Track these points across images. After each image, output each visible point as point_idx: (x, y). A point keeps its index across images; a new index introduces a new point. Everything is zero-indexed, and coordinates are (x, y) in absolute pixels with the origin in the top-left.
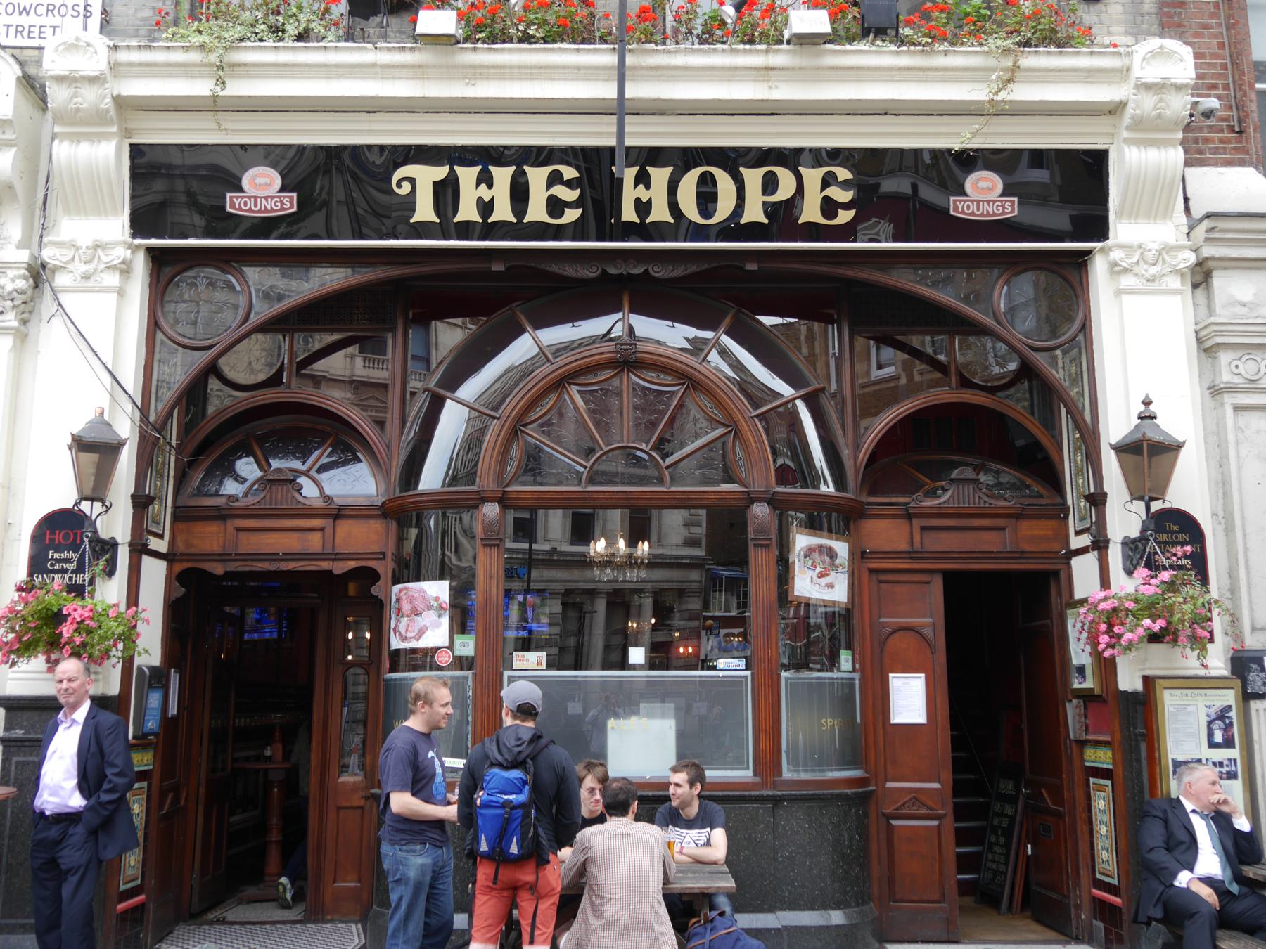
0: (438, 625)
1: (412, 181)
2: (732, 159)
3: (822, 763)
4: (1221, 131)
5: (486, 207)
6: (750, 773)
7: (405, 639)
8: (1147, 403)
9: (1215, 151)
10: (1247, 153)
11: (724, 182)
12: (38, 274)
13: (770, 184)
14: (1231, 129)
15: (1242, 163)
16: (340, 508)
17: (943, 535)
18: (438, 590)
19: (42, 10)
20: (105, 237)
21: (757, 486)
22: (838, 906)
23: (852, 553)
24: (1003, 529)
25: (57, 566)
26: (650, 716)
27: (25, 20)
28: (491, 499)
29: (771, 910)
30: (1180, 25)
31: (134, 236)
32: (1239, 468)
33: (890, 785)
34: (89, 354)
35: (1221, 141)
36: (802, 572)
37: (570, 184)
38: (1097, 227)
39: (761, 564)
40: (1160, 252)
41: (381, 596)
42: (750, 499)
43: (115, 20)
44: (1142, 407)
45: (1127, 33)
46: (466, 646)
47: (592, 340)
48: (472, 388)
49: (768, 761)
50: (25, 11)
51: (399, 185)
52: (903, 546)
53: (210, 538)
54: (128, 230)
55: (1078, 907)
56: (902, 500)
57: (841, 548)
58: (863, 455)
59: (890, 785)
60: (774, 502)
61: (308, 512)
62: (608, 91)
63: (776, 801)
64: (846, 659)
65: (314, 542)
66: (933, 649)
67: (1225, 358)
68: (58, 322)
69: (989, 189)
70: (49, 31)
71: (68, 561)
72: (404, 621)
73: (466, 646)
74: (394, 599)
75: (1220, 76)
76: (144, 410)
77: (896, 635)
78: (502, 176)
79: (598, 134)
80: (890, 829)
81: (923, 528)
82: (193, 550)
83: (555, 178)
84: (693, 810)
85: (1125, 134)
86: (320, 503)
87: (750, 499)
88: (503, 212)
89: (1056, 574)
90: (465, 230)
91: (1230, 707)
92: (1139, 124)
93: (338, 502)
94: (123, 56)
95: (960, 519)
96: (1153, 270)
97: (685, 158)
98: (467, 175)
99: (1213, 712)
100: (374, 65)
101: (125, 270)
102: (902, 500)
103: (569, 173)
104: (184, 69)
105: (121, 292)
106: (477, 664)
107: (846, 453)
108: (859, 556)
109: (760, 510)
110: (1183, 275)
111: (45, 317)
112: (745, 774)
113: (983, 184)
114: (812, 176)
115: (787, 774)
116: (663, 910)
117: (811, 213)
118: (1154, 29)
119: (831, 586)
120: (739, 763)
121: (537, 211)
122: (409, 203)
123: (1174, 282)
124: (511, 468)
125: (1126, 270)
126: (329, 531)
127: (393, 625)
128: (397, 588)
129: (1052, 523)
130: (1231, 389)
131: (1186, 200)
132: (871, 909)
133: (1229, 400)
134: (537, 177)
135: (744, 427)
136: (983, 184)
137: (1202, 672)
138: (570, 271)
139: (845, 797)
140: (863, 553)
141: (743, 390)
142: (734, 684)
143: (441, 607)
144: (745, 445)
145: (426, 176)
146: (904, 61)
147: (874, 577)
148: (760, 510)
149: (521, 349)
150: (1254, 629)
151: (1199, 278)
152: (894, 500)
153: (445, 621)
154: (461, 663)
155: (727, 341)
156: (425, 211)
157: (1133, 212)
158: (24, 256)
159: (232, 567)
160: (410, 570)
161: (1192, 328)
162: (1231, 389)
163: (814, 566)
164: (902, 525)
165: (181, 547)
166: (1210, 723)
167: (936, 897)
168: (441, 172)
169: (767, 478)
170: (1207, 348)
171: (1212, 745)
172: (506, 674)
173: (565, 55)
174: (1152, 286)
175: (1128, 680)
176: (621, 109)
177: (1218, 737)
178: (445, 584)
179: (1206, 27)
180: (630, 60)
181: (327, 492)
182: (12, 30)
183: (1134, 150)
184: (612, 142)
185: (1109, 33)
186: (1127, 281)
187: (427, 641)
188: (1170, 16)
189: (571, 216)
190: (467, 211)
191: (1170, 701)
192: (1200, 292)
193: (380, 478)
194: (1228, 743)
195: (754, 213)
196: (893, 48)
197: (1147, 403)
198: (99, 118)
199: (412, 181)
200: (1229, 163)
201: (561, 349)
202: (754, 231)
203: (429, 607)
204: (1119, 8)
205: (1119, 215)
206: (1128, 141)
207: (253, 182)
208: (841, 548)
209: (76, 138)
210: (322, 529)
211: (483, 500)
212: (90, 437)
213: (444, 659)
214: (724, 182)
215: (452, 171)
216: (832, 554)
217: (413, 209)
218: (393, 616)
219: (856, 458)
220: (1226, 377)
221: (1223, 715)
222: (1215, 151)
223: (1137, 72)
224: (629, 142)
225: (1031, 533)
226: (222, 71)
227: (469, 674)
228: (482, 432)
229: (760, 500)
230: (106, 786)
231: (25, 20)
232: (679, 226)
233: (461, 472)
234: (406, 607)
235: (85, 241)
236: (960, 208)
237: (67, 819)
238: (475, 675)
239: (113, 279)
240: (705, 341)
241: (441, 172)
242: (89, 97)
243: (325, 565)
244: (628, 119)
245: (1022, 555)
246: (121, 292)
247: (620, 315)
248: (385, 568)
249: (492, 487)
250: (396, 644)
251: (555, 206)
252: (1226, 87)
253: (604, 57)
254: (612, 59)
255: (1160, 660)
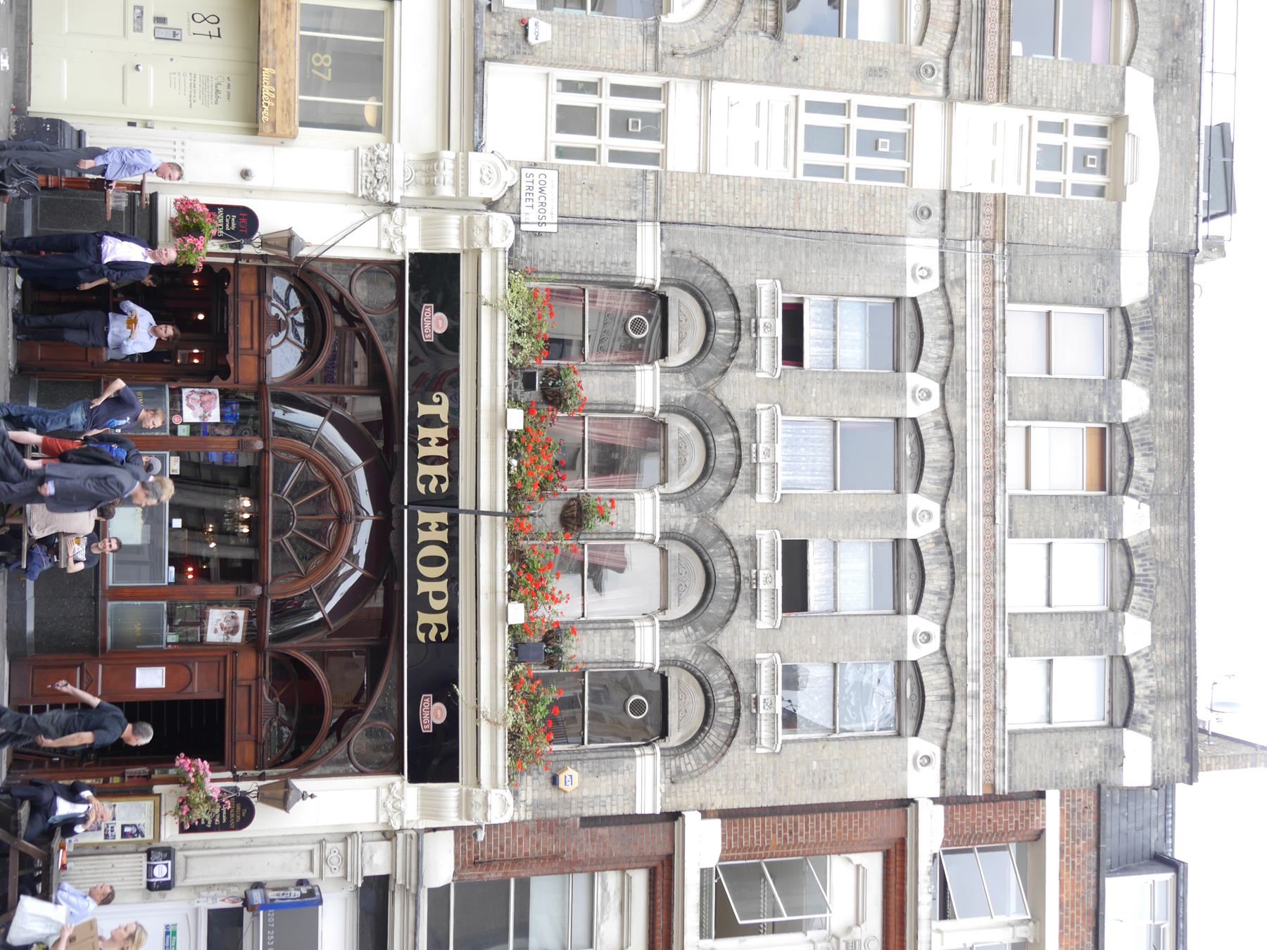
0: (195, 416)
1: (440, 403)
2: (452, 577)
3: (114, 626)
4: (476, 852)
5: (426, 442)
6: (111, 584)
7: (188, 397)
8: (312, 796)
9: (463, 848)
10: (463, 867)
11: (442, 570)
12: (390, 205)
13: (438, 595)
14: (477, 858)
15: (456, 864)
16: (265, 359)
17: (246, 699)
18: (215, 416)
19: (542, 200)
20: (407, 241)
21: (270, 589)
22: (36, 631)
23: (236, 644)
24: (249, 733)
25: (227, 220)
26: (143, 532)
27: (536, 191)
28: (265, 444)
29: (36, 594)
30: (539, 831)
31: (411, 254)
32: (277, 852)
33: (100, 667)
34: (344, 234)
35: (469, 852)
36: (223, 614)
37: (438, 488)
38: (413, 779)
39: (228, 589)
40: (399, 810)
41: (213, 381)
42: (263, 584)
43: (538, 239)
44: (309, 794)
45: (533, 800)
46: (183, 431)
47: (356, 501)
48: (332, 434)
49: (118, 594)
50: (542, 190)
51: (437, 396)
52: (239, 675)
53: (247, 285)
54: (414, 252)
55: (27, 773)
56: (267, 675)
57: (238, 638)
58: (294, 653)
59: (100, 667)
60: (262, 598)
61: (261, 341)
62: (484, 506)
63: (96, 598)
64: (173, 638)
65: (245, 344)
66: (178, 693)
67: (340, 846)
68: (361, 217)
69: (437, 716)
70: (530, 203)
71: (230, 225)
72: (198, 397)
73: (183, 431)
74: (211, 390)
75: (508, 853)
76: (317, 259)
77: (187, 672)
78: (443, 451)
79: (465, 501)
80: (76, 667)
81: (250, 686)
82: (240, 277)
83: (441, 479)
84: (95, 551)
85: (464, 789)
86: (267, 347)
87: (263, 584)
88: (423, 451)
89: (223, 764)
90: (414, 432)
91: (143, 836)
92: (469, 794)
93: (268, 357)
94: (501, 255)
95: (254, 708)
96: (389, 806)
97: (452, 546)
98: (443, 433)
99: (141, 827)
100: (497, 385)
101: (390, 250)
102: (267, 675)
103: (444, 487)
104: (494, 287)
105: (378, 248)
106: (174, 437)
107: (294, 643)
108: (233, 649)
109: (258, 590)
110: (387, 824)
111: (364, 208)
112: (110, 581)
113: (439, 712)
114: (443, 619)
115: (110, 604)
116: (54, 532)
117: (423, 618)
118: (536, 815)
119: (216, 631)
120: (115, 579)
121: (423, 470)
122: (428, 401)
123: (383, 819)
124: (283, 455)
125: (390, 790)
126: (251, 352)
127: (196, 390)
128: (216, 392)
129: (252, 761)
130: (322, 848)
131: (434, 830)
132: (31, 652)
133: (316, 847)
134: (442, 470)
135: (305, 582)
136: (439, 712)
137: (163, 813)
138: (393, 487)
139: (97, 635)
140: (236, 652)
141: (328, 581)
142: (160, 574)
143: (205, 417)
144: (294, 582)
145: (442, 411)
146: (500, 666)
147: (222, 659)
148: (258, 590)
149: (354, 457)
150: (186, 858)
151: (388, 835)
152: (267, 670)
153: (198, 420)
154: (174, 430)
155: (357, 575)
156: (423, 410)
157: (424, 797)
158: (396, 200)
159: (231, 299)
160: (226, 398)
161: (359, 830)
162: (322, 848)
163: (227, 621)
164: (252, 675)
165: (242, 270)
166: (135, 826)
167: (35, 692)
168: (445, 419)
169: (275, 594)
170: (347, 837)
171: (123, 827)
172: (168, 453)
173: (503, 486)
174: (381, 805)
175: (157, 789)
176: (477, 513)
177: (127, 830)
178: (218, 420)
179: (538, 845)
180: (500, 519)
181: (273, 351)
182: (531, 184)
183: (457, 794)
184: (461, 507)
185: (533, 790)
186: (384, 792)
187: (186, 410)
188: (545, 824)
189: (421, 488)
190: (423, 432)
191: (147, 804)
192: (380, 836)
193: (282, 380)
194: (124, 835)
195: (423, 587)
196: (507, 660)
197: (312, 796)
198: (470, 241)
199: (440, 403)
200: (456, 856)
201: (351, 483)
202: (413, 587)
203: (205, 412)
204: (549, 796)
205: (422, 789)
206: (461, 790)
207: (438, 319)
208: (238, 638)
209: (461, 227)
210: (252, 348)
211: (264, 440)
212: (294, 243)
213: (176, 420)
214: (442, 570)
215: (443, 424)
216: (234, 632)
217: (423, 403)
218: (201, 390)
219: (291, 648)
220: (329, 846)
221: (139, 833)
222: (463, 848)
223: (494, 791)
224: (461, 516)
225: (246, 751)
226: (494, 308)
227: (168, 433)
228: (300, 437)
229: (263, 590)
230: (111, 271)
231: (536, 191)
232: (415, 547)
233: (285, 428)
234: (206, 398)
235: (405, 231)
236: (426, 700)
237: (99, 252)
238: (167, 436)
239: (385, 245)
240: (357, 563)
241: (445, 419)
242: (479, 238)
243: (231, 350)
244: (473, 516)
245: (234, 744)
246: (378, 248)
247: (371, 514)
248: (229, 384)
249: (272, 445)
250: (185, 392)
251: (426, 479)
252: (502, 856)
253: (502, 505)
254: (500, 509)
255: (170, 802)
